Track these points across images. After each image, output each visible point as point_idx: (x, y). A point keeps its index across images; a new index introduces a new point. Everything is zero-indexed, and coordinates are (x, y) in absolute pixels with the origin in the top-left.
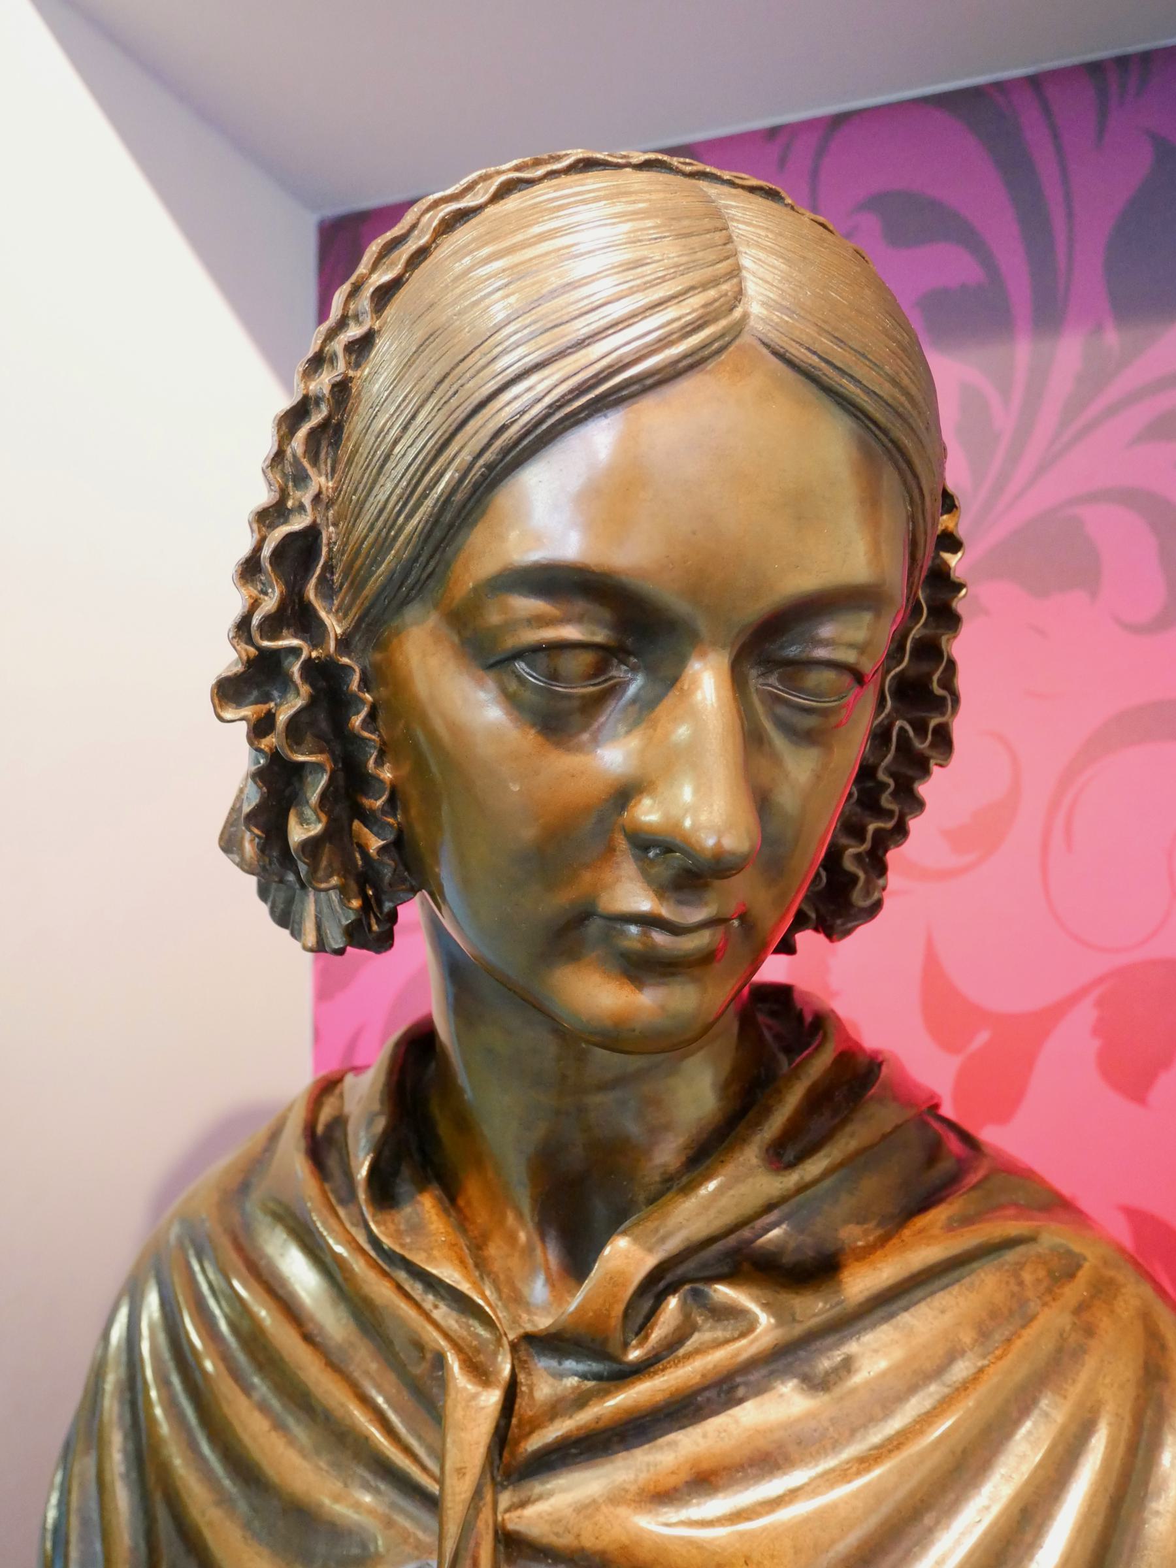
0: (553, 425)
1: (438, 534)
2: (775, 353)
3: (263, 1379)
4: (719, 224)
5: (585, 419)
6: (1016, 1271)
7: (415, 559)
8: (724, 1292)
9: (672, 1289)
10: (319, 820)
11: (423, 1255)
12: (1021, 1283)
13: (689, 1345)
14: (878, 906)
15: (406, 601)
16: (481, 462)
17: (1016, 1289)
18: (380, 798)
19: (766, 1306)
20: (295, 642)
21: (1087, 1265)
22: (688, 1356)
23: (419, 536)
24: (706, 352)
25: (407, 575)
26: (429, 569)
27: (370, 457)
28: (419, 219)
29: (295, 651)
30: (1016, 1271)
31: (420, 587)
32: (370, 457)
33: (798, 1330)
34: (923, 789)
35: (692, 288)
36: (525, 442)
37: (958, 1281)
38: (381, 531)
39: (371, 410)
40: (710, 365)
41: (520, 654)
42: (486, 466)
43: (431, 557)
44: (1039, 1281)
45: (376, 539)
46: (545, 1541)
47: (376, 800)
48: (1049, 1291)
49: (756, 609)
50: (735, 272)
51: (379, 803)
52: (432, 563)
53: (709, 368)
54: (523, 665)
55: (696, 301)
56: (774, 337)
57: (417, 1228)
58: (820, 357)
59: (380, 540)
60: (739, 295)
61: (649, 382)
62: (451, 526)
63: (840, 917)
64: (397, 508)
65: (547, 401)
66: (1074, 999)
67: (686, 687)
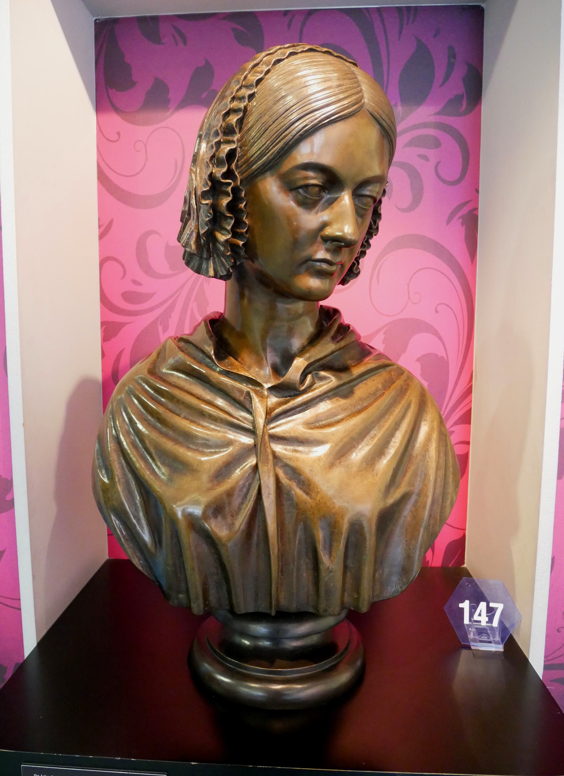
0: (319, 126)
1: (282, 152)
2: (370, 113)
3: (128, 451)
4: (354, 77)
5: (327, 125)
6: (390, 372)
7: (273, 159)
8: (323, 373)
9: (310, 373)
10: (230, 234)
11: (236, 370)
12: (391, 375)
13: (315, 386)
14: (359, 273)
15: (266, 171)
16: (299, 134)
17: (390, 376)
18: (244, 229)
19: (334, 376)
20: (230, 181)
21: (405, 372)
22: (315, 389)
23: (277, 152)
24: (356, 111)
25: (268, 164)
26: (277, 162)
27: (260, 129)
28: (263, 59)
29: (229, 184)
30: (390, 372)
31: (271, 168)
32: (260, 129)
33: (342, 382)
34: (371, 241)
35: (353, 94)
36: (311, 130)
37: (376, 374)
38: (263, 150)
39: (260, 116)
40: (356, 115)
41: (301, 187)
42: (300, 135)
43: (278, 159)
44: (395, 374)
45: (261, 152)
46: (281, 435)
47: (243, 229)
48: (398, 377)
49: (361, 178)
50: (361, 91)
51: (245, 230)
52: (278, 161)
53: (356, 115)
54: (301, 190)
55: (354, 97)
56: (370, 110)
57: (231, 365)
58: (379, 115)
59: (263, 153)
60: (362, 97)
61: (343, 117)
62: (286, 150)
63: (348, 276)
64: (270, 145)
65: (319, 119)
66: (377, 332)
67: (342, 198)
